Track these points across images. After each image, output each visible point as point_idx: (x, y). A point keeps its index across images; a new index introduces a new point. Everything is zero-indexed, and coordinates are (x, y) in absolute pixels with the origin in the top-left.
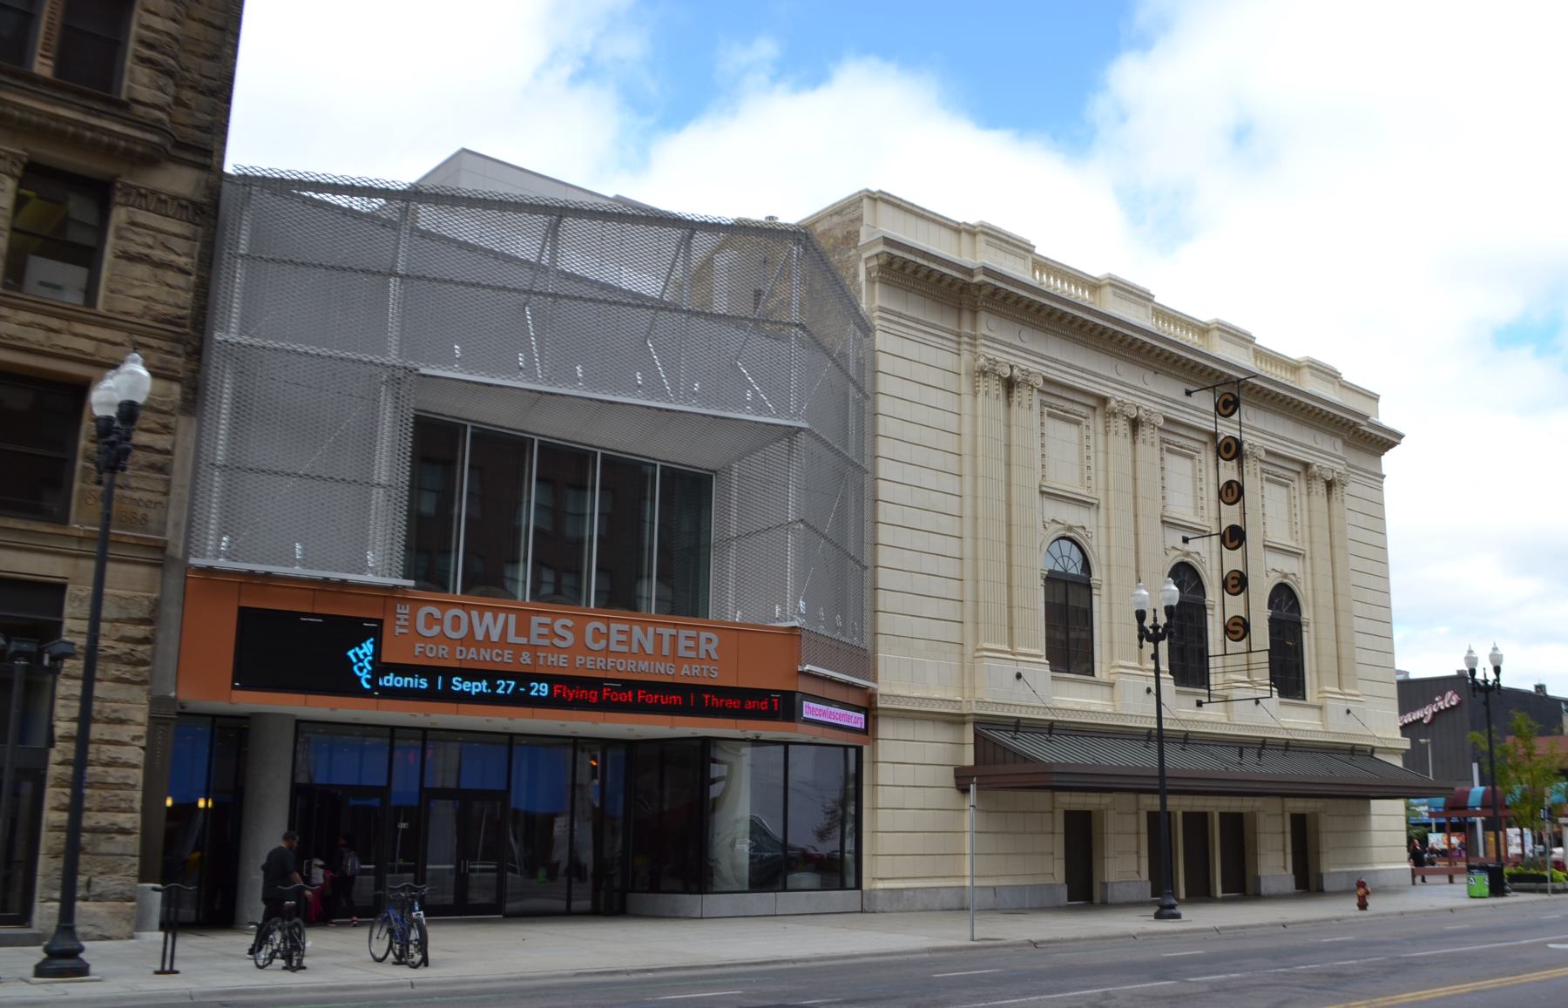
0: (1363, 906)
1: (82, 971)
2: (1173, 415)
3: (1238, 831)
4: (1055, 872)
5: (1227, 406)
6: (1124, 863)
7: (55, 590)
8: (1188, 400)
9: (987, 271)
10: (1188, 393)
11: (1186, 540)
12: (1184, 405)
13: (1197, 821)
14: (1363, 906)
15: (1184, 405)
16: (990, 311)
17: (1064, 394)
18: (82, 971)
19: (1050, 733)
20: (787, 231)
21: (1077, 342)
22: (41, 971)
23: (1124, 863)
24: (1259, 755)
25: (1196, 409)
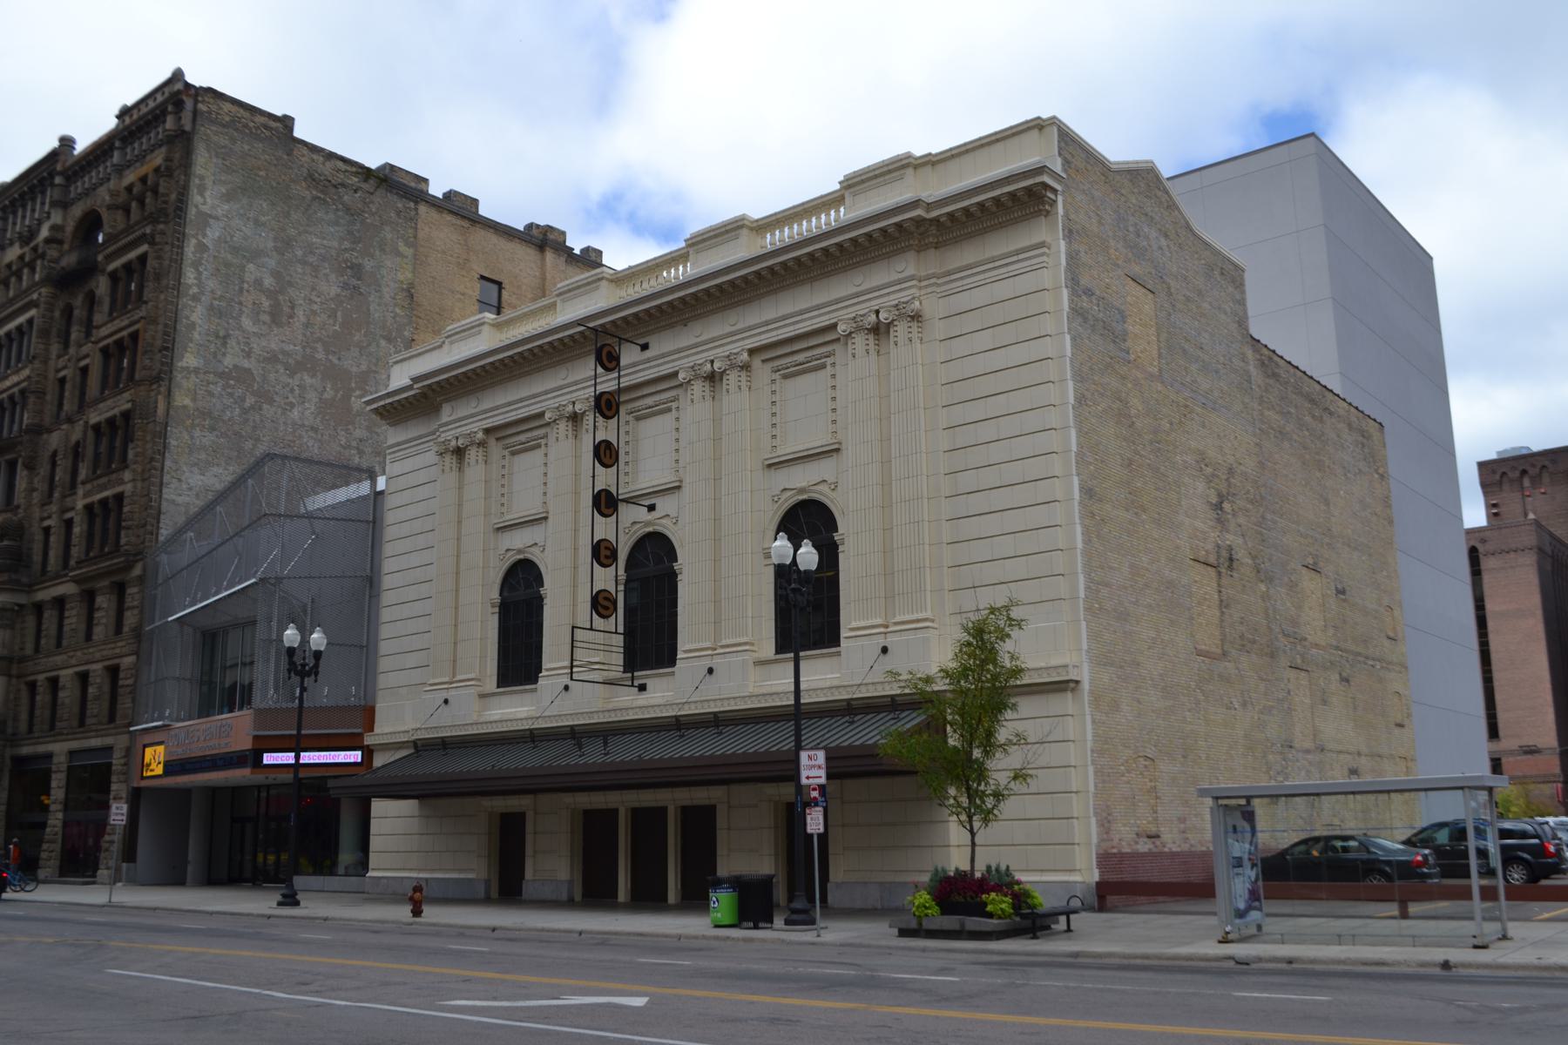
0: (417, 912)
1: (297, 903)
2: (488, 423)
3: (700, 829)
4: (476, 869)
5: (609, 361)
6: (551, 862)
7: (108, 749)
8: (648, 354)
9: (415, 380)
10: (645, 347)
11: (652, 508)
12: (649, 360)
13: (648, 823)
14: (417, 912)
15: (649, 360)
16: (447, 400)
17: (659, 388)
18: (297, 903)
19: (679, 729)
20: (1103, 164)
21: (775, 291)
22: (280, 904)
23: (551, 862)
24: (605, 743)
25: (663, 356)
